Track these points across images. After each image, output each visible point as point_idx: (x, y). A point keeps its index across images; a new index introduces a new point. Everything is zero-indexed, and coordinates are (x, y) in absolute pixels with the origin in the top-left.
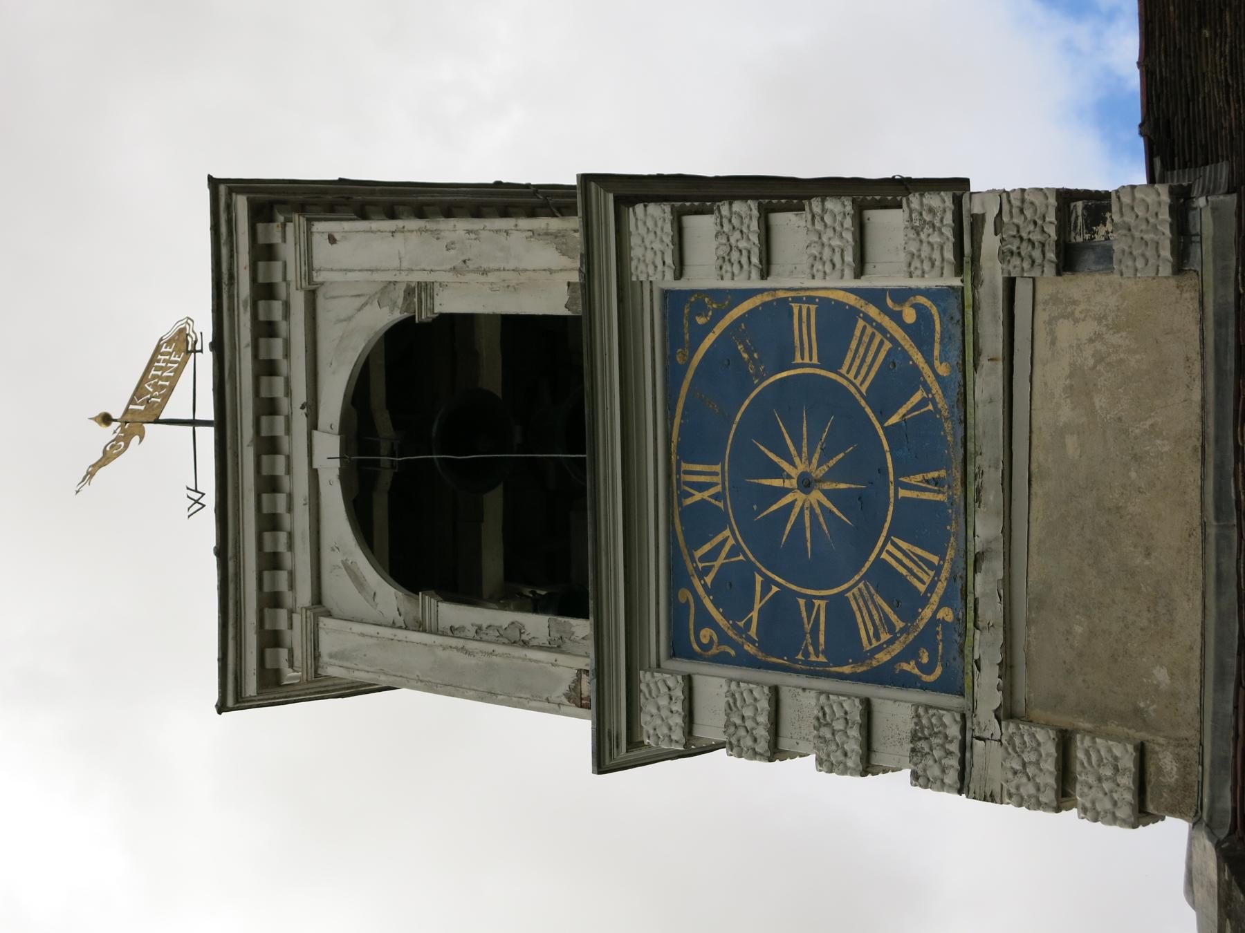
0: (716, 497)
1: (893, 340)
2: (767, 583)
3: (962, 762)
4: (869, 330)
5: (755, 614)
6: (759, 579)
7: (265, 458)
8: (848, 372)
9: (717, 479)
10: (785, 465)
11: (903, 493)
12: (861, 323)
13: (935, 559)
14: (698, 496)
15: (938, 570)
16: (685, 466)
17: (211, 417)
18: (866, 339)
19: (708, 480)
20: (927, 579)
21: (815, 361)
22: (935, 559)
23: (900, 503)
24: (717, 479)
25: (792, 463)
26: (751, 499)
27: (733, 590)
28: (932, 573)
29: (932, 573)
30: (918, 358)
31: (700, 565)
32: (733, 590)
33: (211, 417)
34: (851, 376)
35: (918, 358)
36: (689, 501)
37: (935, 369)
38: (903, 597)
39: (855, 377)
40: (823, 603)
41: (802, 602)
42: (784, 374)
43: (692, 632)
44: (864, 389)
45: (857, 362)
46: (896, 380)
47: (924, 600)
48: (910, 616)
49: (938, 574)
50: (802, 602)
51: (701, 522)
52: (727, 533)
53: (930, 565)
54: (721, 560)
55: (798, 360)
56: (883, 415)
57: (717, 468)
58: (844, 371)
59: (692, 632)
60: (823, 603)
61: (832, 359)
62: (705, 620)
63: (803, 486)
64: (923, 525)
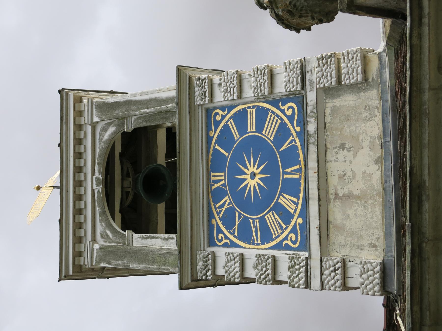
0: (223, 185)
1: (282, 119)
2: (240, 215)
3: (307, 271)
4: (273, 116)
5: (236, 226)
6: (237, 214)
7: (77, 202)
8: (265, 133)
9: (223, 178)
10: (246, 170)
11: (286, 176)
12: (270, 114)
13: (295, 200)
14: (216, 186)
15: (297, 204)
16: (212, 174)
17: (59, 186)
18: (270, 133)
19: (220, 177)
20: (294, 208)
21: (254, 130)
22: (295, 200)
23: (285, 180)
24: (223, 178)
25: (248, 169)
26: (234, 183)
27: (230, 213)
28: (295, 206)
29: (295, 206)
30: (290, 125)
31: (218, 210)
32: (228, 221)
33: (59, 186)
34: (266, 135)
35: (290, 125)
36: (213, 187)
37: (294, 129)
38: (286, 216)
39: (268, 135)
40: (258, 220)
41: (251, 221)
42: (236, 207)
43: (215, 236)
44: (272, 139)
45: (269, 126)
46: (283, 133)
47: (292, 216)
48: (287, 223)
49: (297, 206)
50: (251, 221)
51: (218, 195)
52: (227, 198)
53: (294, 202)
54: (226, 207)
55: (249, 131)
56: (278, 148)
57: (223, 174)
58: (263, 133)
59: (215, 236)
60: (258, 220)
61: (260, 128)
62: (219, 231)
63: (252, 177)
64: (291, 188)
